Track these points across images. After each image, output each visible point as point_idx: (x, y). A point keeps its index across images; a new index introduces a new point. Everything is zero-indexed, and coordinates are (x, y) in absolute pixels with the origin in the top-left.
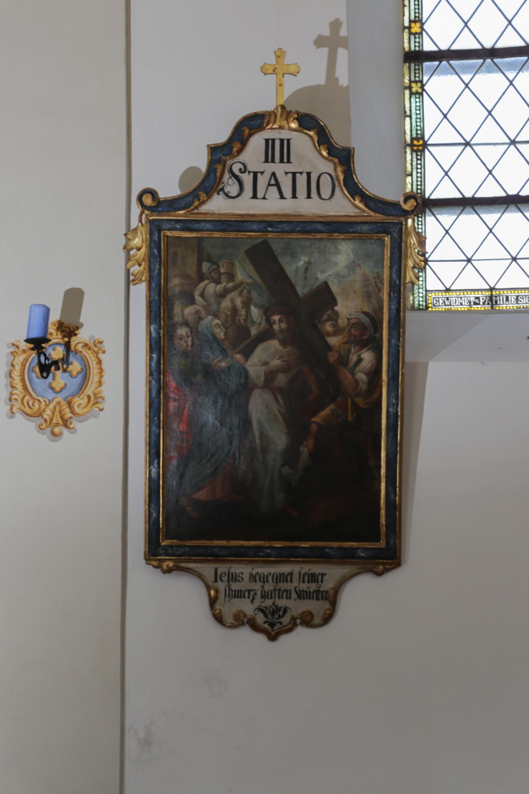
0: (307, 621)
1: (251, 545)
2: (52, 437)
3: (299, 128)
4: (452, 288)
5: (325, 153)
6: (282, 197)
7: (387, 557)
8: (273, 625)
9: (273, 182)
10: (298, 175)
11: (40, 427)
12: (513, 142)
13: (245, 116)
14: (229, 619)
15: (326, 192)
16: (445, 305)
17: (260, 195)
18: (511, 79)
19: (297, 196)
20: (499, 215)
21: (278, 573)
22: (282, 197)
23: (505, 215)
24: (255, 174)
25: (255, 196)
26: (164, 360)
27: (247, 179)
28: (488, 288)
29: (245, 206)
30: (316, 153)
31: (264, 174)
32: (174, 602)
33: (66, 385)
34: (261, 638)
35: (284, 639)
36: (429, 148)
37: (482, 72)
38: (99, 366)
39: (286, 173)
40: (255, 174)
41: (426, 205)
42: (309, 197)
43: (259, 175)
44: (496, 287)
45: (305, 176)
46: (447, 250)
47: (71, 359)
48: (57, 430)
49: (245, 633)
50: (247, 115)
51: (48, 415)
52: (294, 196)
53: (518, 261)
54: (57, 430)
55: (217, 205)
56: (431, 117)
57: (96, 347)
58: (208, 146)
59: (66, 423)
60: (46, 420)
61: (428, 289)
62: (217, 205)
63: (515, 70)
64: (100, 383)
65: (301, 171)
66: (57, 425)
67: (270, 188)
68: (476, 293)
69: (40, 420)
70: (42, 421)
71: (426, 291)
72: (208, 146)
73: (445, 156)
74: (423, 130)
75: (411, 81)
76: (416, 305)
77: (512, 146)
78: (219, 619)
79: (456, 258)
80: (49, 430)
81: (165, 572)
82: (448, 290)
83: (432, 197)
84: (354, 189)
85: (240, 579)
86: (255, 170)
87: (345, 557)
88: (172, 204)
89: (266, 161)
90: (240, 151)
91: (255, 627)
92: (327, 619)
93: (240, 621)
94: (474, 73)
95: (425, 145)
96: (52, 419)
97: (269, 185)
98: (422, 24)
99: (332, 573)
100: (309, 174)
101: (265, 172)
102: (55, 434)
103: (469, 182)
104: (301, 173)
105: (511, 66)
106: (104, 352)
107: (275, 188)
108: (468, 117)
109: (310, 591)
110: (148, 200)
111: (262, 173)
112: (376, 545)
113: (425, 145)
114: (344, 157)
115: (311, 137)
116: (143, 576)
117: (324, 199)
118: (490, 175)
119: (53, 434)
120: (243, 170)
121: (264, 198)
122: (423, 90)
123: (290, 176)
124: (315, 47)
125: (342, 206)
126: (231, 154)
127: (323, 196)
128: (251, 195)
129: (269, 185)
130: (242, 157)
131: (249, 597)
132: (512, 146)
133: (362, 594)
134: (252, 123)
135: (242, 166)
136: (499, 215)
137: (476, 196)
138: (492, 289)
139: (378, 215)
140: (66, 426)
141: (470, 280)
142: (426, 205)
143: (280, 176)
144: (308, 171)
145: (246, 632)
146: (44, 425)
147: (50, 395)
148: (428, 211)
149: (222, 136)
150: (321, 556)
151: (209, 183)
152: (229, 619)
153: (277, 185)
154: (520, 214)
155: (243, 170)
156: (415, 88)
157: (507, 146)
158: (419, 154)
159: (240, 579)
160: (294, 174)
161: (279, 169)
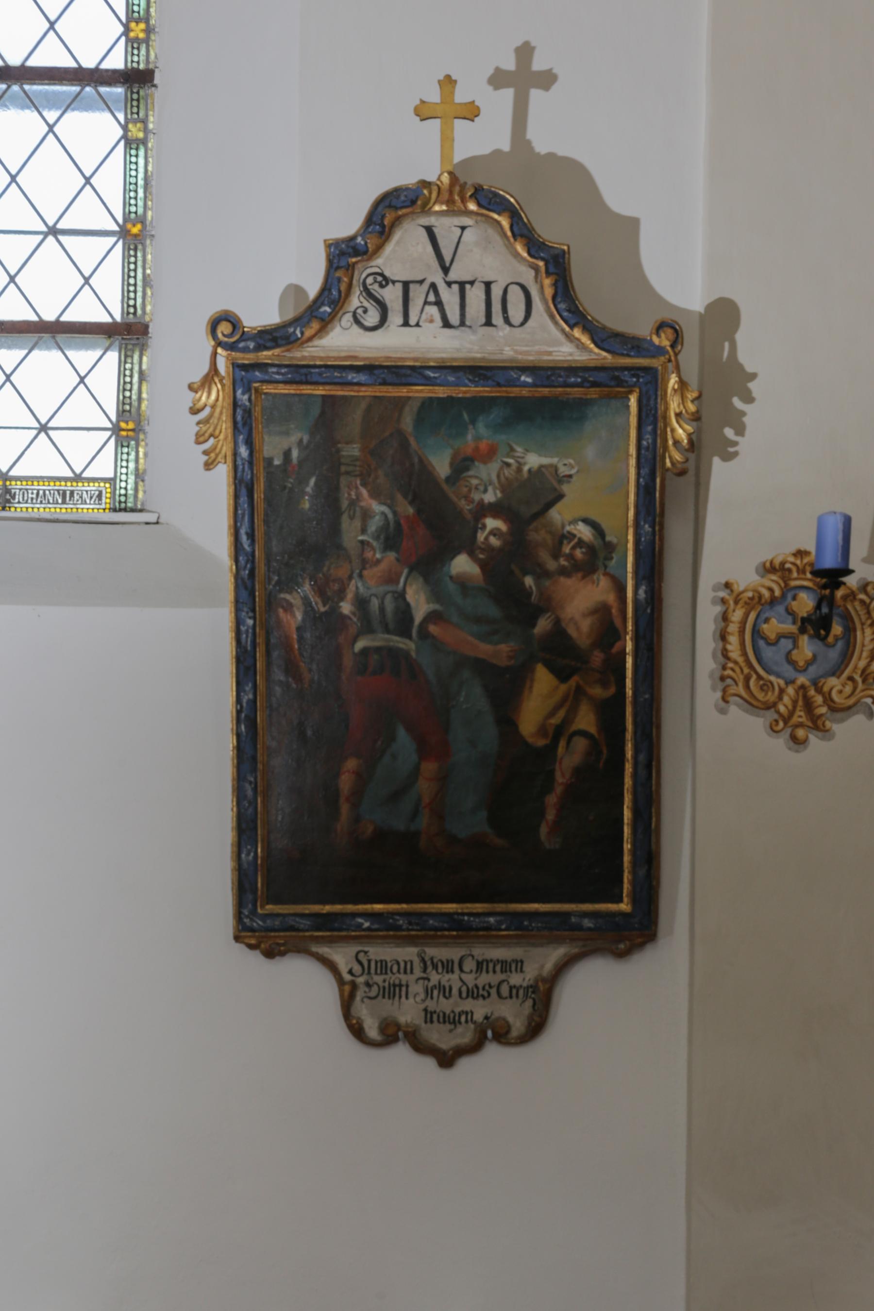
1: (433, 911)
2: (791, 744)
4: (84, 475)
7: (635, 931)
9: (432, 298)
11: (773, 729)
12: (54, 231)
14: (372, 1031)
15: (517, 312)
17: (413, 321)
18: (51, 122)
20: (99, 353)
22: (446, 324)
23: (36, 353)
29: (394, 342)
30: (571, 250)
34: (429, 1063)
37: (73, 110)
40: (406, 285)
43: (468, 286)
48: (801, 733)
51: (785, 706)
52: (463, 323)
53: (51, 433)
54: (801, 733)
55: (343, 340)
63: (58, 108)
65: (419, 278)
66: (800, 725)
68: (58, 483)
69: (771, 715)
70: (776, 716)
77: (51, 238)
78: (357, 1031)
80: (788, 731)
82: (78, 478)
86: (404, 279)
87: (558, 928)
88: (270, 337)
93: (391, 1034)
95: (123, 233)
96: (791, 713)
98: (125, 137)
99: (542, 959)
100: (488, 285)
104: (472, 283)
105: (52, 102)
110: (224, 328)
113: (123, 233)
117: (514, 326)
118: (12, 285)
119: (794, 738)
125: (549, 341)
129: (426, 303)
131: (517, 996)
132: (51, 238)
134: (391, 210)
136: (99, 353)
137: (62, 319)
139: (604, 354)
142: (127, 333)
144: (486, 279)
145: (402, 1052)
146: (781, 724)
149: (349, 223)
150: (523, 929)
153: (439, 303)
154: (60, 353)
157: (41, 237)
158: (135, 45)
159: (486, 994)
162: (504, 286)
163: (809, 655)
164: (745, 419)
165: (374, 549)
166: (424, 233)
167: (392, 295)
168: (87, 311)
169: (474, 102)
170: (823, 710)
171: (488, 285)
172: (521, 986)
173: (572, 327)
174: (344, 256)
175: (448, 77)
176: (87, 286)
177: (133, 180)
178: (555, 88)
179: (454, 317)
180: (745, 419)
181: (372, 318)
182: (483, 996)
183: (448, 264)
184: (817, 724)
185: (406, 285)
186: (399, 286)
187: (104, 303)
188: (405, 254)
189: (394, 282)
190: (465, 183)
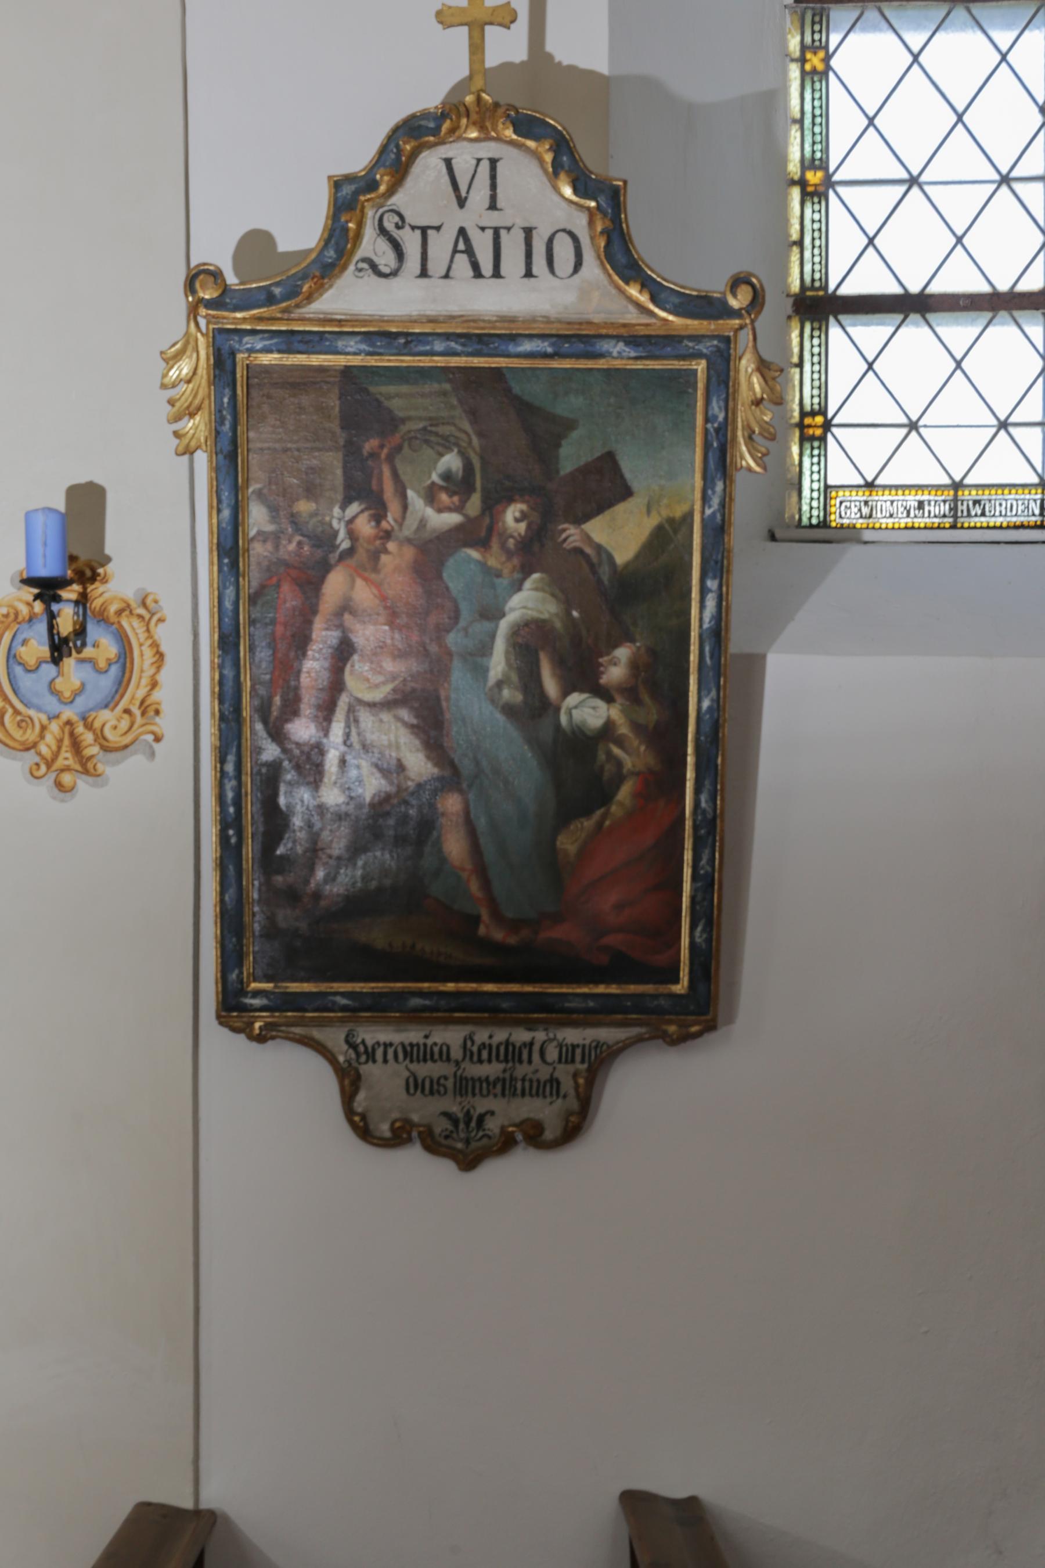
0: (534, 1136)
3: (482, 136)
5: (568, 191)
6: (478, 274)
7: (696, 1011)
8: (467, 1145)
9: (461, 246)
16: (861, 517)
19: (503, 273)
22: (478, 274)
24: (496, 231)
27: (411, 242)
28: (947, 481)
31: (512, 231)
32: (275, 1096)
33: (83, 685)
34: (446, 1167)
36: (840, 189)
38: (155, 650)
39: (483, 229)
40: (424, 230)
41: (820, 307)
44: (967, 481)
46: (869, 403)
47: (94, 631)
48: (67, 779)
49: (413, 1158)
51: (48, 746)
52: (497, 274)
54: (67, 779)
55: (353, 297)
56: (843, 123)
57: (147, 609)
58: (330, 178)
59: (86, 767)
60: (43, 758)
61: (830, 482)
62: (353, 297)
64: (154, 685)
66: (67, 769)
67: (458, 256)
69: (31, 757)
70: (37, 759)
71: (827, 487)
72: (330, 178)
73: (870, 205)
74: (826, 150)
75: (804, 48)
76: (805, 521)
79: (898, 422)
80: (52, 776)
81: (261, 1039)
83: (845, 290)
84: (623, 259)
90: (391, 191)
91: (433, 1145)
92: (572, 1130)
93: (398, 1137)
94: (934, 28)
96: (56, 755)
98: (828, 58)
100: (528, 232)
102: (62, 786)
103: (913, 258)
106: (161, 620)
108: (916, 124)
109: (538, 1081)
111: (438, 228)
113: (829, 183)
114: (607, 199)
116: (216, 1037)
119: (59, 785)
120: (400, 223)
121: (447, 276)
122: (828, 68)
123: (490, 233)
129: (455, 251)
130: (398, 200)
133: (649, 1090)
134: (413, 135)
135: (397, 219)
138: (957, 486)
140: (86, 772)
141: (914, 466)
142: (820, 307)
143: (474, 234)
147: (51, 704)
148: (832, 320)
149: (357, 158)
153: (470, 251)
155: (400, 223)
156: (815, 61)
160: (496, 231)
162: (546, 239)
163: (77, 684)
168: (870, 333)
169: (509, 3)
170: (94, 750)
171: (528, 232)
175: (439, 14)
176: (871, 129)
177: (816, 226)
179: (487, 268)
181: (386, 259)
183: (463, 194)
184: (86, 767)
187: (847, 344)
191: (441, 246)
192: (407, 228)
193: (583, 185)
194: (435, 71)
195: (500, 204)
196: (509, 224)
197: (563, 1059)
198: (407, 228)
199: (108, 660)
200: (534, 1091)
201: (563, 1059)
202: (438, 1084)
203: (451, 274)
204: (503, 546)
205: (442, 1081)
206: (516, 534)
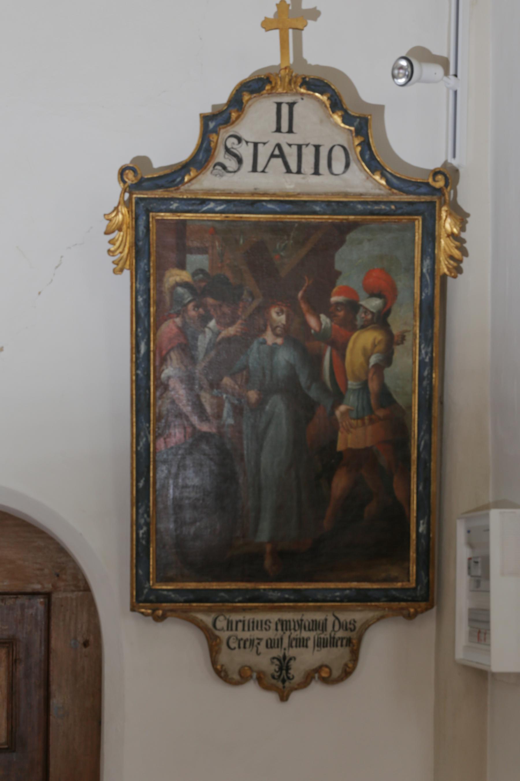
9: (277, 152)
10: (304, 150)
13: (122, 167)
15: (338, 166)
17: (260, 168)
21: (310, 620)
24: (256, 145)
25: (254, 169)
26: (413, 293)
29: (243, 181)
31: (267, 145)
35: (296, 697)
39: (290, 145)
42: (316, 172)
43: (304, 147)
45: (312, 149)
50: (246, 79)
52: (299, 172)
55: (208, 182)
62: (208, 182)
67: (274, 160)
72: (201, 115)
78: (222, 674)
84: (373, 164)
85: (267, 627)
89: (278, 130)
92: (347, 673)
97: (272, 156)
100: (317, 148)
101: (269, 143)
104: (307, 145)
107: (279, 161)
111: (264, 144)
112: (406, 585)
115: (322, 103)
117: (339, 145)
121: (263, 171)
124: (318, 8)
125: (357, 182)
126: (228, 122)
127: (230, 169)
128: (250, 168)
129: (272, 156)
134: (257, 85)
143: (286, 149)
144: (317, 143)
151: (202, 157)
152: (236, 677)
153: (282, 155)
159: (267, 627)
160: (300, 147)
161: (283, 139)
164: (468, 219)
165: (183, 405)
166: (275, 106)
167: (246, 152)
171: (317, 148)
172: (247, 640)
173: (373, 172)
174: (216, 121)
178: (319, 19)
179: (294, 167)
180: (468, 219)
182: (266, 629)
185: (256, 145)
186: (251, 146)
188: (258, 120)
189: (247, 142)
190: (113, 262)
191: (264, 153)
192: (244, 143)
193: (347, 119)
194: (265, 54)
195: (294, 129)
196: (307, 143)
197: (269, 646)
198: (244, 143)
199: (364, 349)
200: (325, 645)
201: (269, 646)
202: (266, 624)
203: (266, 170)
204: (274, 330)
205: (268, 623)
206: (280, 324)
